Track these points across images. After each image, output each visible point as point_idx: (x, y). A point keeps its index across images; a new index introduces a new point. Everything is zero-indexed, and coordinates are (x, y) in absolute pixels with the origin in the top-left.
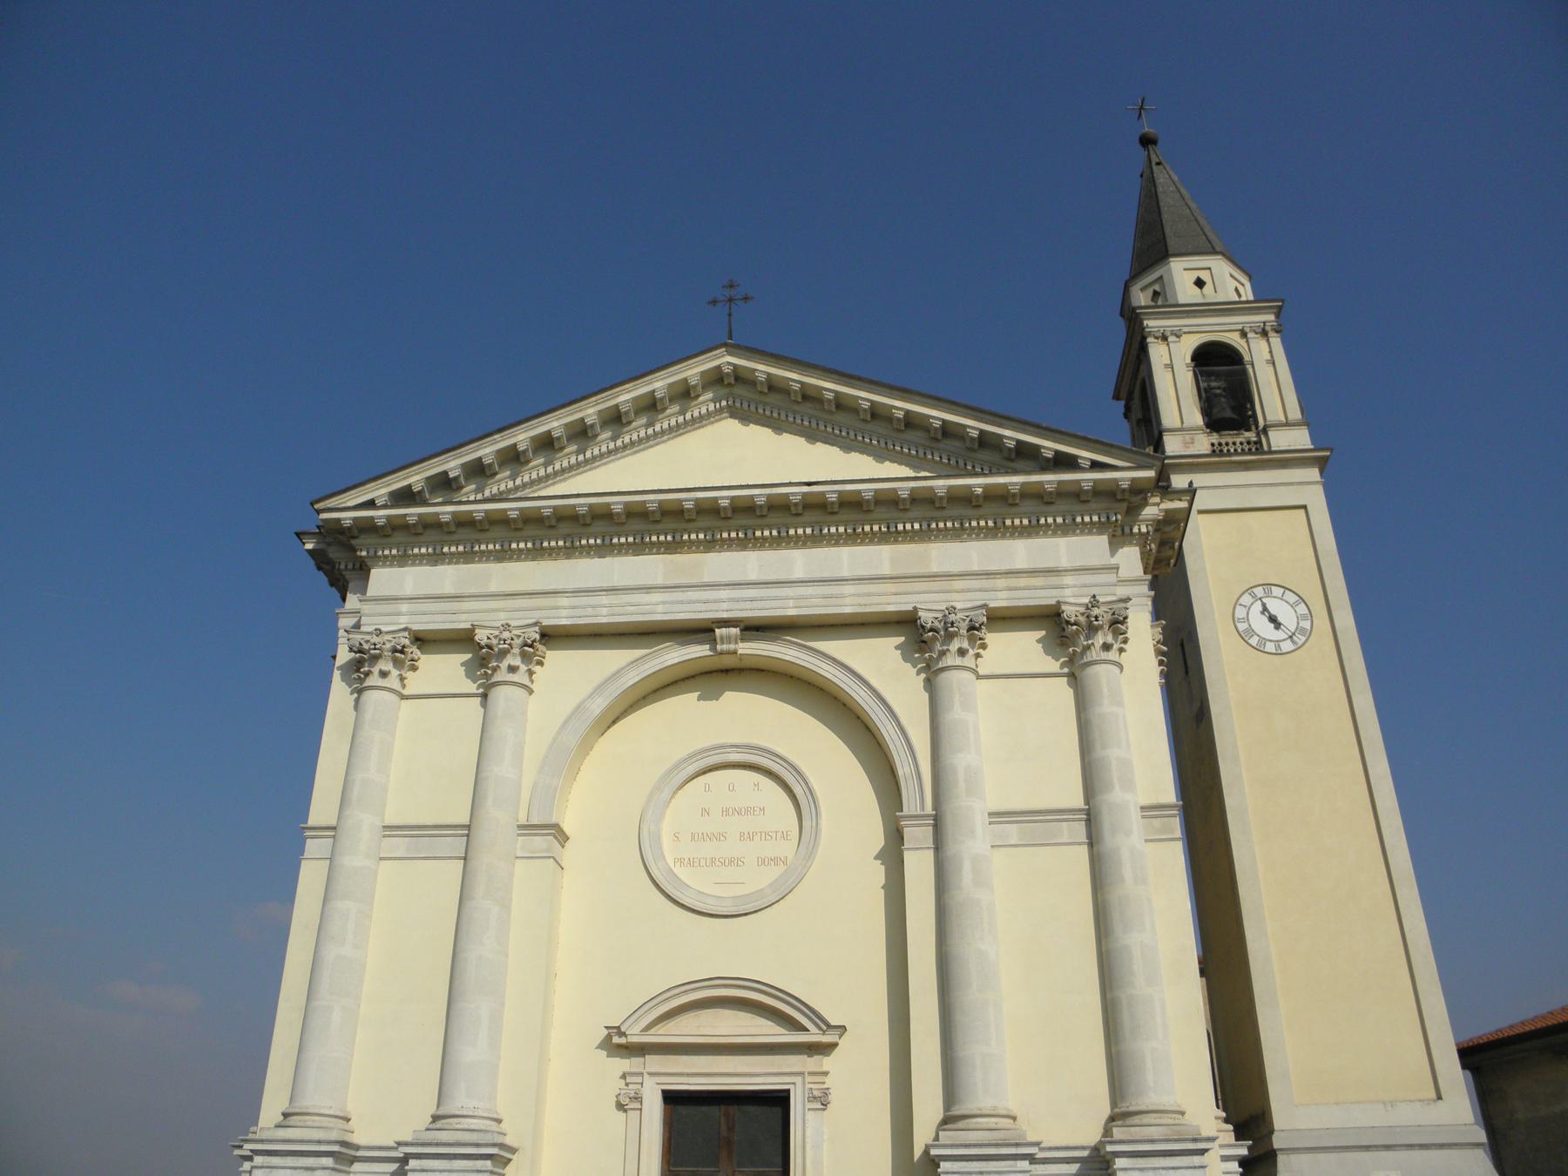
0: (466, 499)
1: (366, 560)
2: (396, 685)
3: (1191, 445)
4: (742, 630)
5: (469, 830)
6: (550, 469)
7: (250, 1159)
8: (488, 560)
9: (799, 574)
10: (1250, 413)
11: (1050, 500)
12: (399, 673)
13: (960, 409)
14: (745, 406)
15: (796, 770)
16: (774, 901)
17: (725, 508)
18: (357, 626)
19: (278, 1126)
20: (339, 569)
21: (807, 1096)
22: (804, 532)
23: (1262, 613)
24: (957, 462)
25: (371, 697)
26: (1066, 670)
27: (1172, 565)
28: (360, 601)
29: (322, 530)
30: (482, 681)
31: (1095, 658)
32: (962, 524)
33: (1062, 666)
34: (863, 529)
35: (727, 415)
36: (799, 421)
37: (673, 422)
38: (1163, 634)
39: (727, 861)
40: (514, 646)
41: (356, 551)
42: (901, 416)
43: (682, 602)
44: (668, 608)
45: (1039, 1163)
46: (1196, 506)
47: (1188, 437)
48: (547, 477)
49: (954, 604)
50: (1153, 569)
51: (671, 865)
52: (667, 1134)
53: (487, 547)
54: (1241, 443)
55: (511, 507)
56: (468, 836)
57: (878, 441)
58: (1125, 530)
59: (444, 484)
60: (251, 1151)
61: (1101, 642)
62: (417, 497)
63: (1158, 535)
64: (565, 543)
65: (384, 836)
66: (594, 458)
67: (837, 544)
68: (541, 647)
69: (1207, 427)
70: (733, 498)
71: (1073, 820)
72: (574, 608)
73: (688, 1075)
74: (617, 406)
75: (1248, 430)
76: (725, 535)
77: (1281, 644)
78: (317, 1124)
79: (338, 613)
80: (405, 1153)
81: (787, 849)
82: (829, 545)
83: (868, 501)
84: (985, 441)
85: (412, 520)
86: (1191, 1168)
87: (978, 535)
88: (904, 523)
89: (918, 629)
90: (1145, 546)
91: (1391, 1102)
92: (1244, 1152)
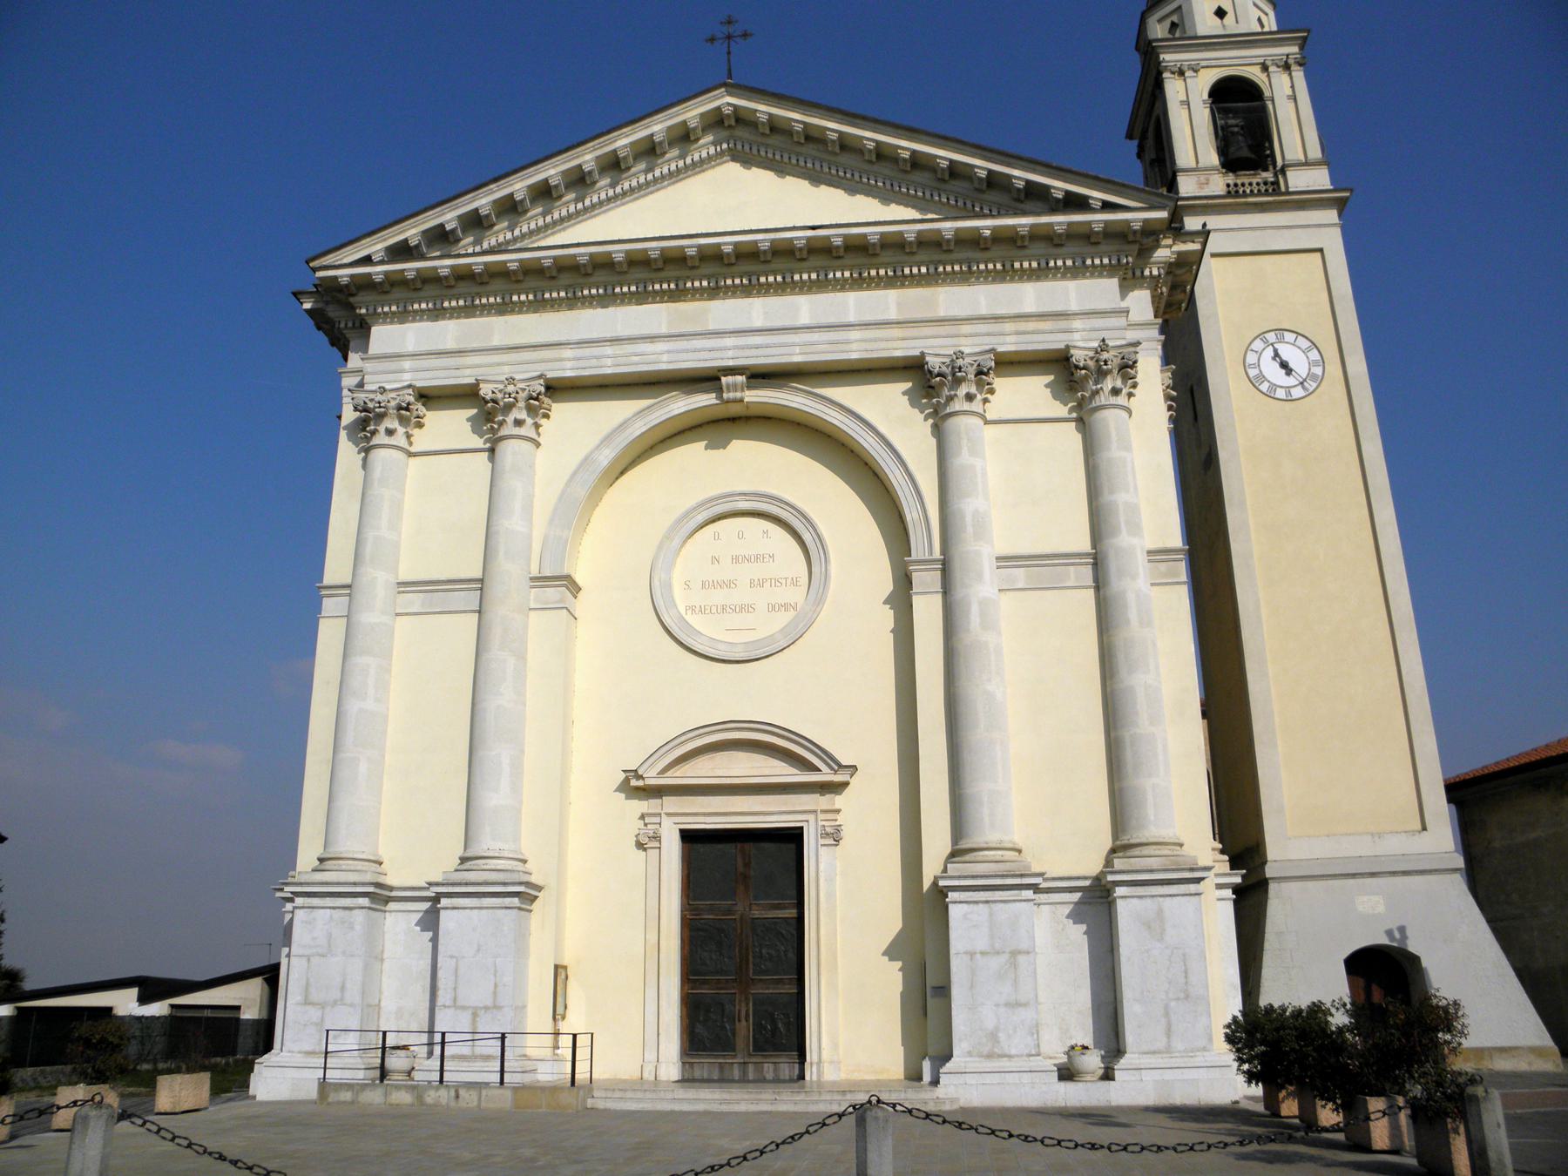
2: (403, 442)
8: (489, 314)
18: (361, 385)
23: (1274, 359)
33: (1070, 411)
35: (729, 158)
43: (687, 351)
47: (1202, 179)
49: (962, 349)
50: (1165, 313)
51: (683, 611)
52: (686, 872)
56: (481, 589)
59: (441, 237)
60: (292, 893)
66: (593, 206)
67: (843, 289)
72: (579, 359)
73: (704, 814)
75: (1266, 170)
81: (797, 595)
82: (834, 290)
84: (994, 182)
85: (410, 275)
88: (911, 267)
90: (1156, 290)
92: (1238, 880)
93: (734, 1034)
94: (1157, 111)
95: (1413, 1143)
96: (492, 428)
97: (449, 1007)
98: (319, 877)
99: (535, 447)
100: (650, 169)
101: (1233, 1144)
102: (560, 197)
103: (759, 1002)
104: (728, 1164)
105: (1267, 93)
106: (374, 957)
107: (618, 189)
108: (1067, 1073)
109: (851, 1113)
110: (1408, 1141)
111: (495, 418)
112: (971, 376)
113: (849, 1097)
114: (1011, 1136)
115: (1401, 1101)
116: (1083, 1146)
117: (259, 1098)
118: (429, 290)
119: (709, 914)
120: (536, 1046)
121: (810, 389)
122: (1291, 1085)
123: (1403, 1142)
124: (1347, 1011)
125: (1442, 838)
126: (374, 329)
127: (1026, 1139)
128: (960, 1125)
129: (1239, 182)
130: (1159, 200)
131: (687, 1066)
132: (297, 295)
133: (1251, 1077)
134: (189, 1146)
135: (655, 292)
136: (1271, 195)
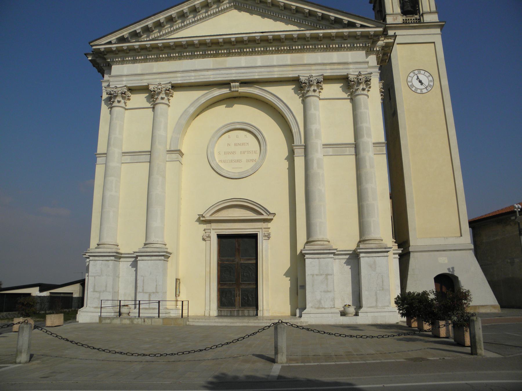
0: (143, 40)
1: (110, 63)
2: (123, 105)
3: (396, 20)
4: (240, 84)
5: (151, 153)
6: (172, 29)
7: (88, 258)
8: (152, 62)
9: (259, 64)
10: (417, 8)
11: (346, 38)
12: (124, 101)
13: (315, 6)
14: (240, 5)
15: (259, 131)
16: (252, 173)
17: (233, 41)
18: (109, 86)
19: (96, 248)
20: (101, 66)
21: (263, 235)
22: (261, 49)
23: (417, 79)
24: (314, 25)
25: (115, 109)
26: (349, 97)
27: (387, 62)
28: (109, 77)
29: (94, 53)
30: (152, 103)
31: (359, 93)
32: (315, 47)
33: (348, 96)
34: (281, 48)
35: (233, 8)
36: (259, 10)
37: (215, 11)
38: (383, 85)
39: (236, 160)
40: (163, 90)
41: (106, 59)
42: (295, 8)
43: (219, 74)
44: (215, 76)
45: (336, 255)
46: (396, 42)
47: (395, 17)
48: (171, 31)
49: (312, 74)
50: (381, 63)
51: (218, 162)
53: (152, 57)
54: (414, 19)
55: (159, 42)
56: (150, 154)
57: (286, 17)
58: (371, 50)
59: (135, 35)
60: (89, 255)
61: (362, 88)
62: (126, 40)
63: (383, 51)
64: (178, 55)
65: (123, 156)
66: (187, 25)
67: (272, 54)
68: (172, 91)
69: (402, 13)
70: (236, 38)
71: (351, 147)
72: (183, 77)
73: (225, 229)
74: (195, 5)
75: (416, 15)
76: (234, 51)
77: (423, 90)
78: (109, 247)
79: (102, 82)
80: (137, 255)
81: (256, 156)
82: (269, 54)
83: (283, 38)
84: (324, 17)
85: (125, 48)
86: (383, 256)
88: (295, 46)
89: (300, 83)
90: (378, 55)
91: (447, 237)
92: (400, 252)
93: (235, 301)
96: (153, 100)
97: (141, 292)
106: (116, 276)
108: (343, 314)
110: (451, 334)
111: (154, 97)
112: (315, 84)
114: (325, 333)
115: (450, 322)
116: (348, 336)
119: (226, 262)
120: (170, 305)
122: (415, 317)
124: (434, 294)
125: (467, 239)
128: (308, 329)
133: (403, 315)
134: (57, 336)
135: (208, 54)
136: (417, 23)
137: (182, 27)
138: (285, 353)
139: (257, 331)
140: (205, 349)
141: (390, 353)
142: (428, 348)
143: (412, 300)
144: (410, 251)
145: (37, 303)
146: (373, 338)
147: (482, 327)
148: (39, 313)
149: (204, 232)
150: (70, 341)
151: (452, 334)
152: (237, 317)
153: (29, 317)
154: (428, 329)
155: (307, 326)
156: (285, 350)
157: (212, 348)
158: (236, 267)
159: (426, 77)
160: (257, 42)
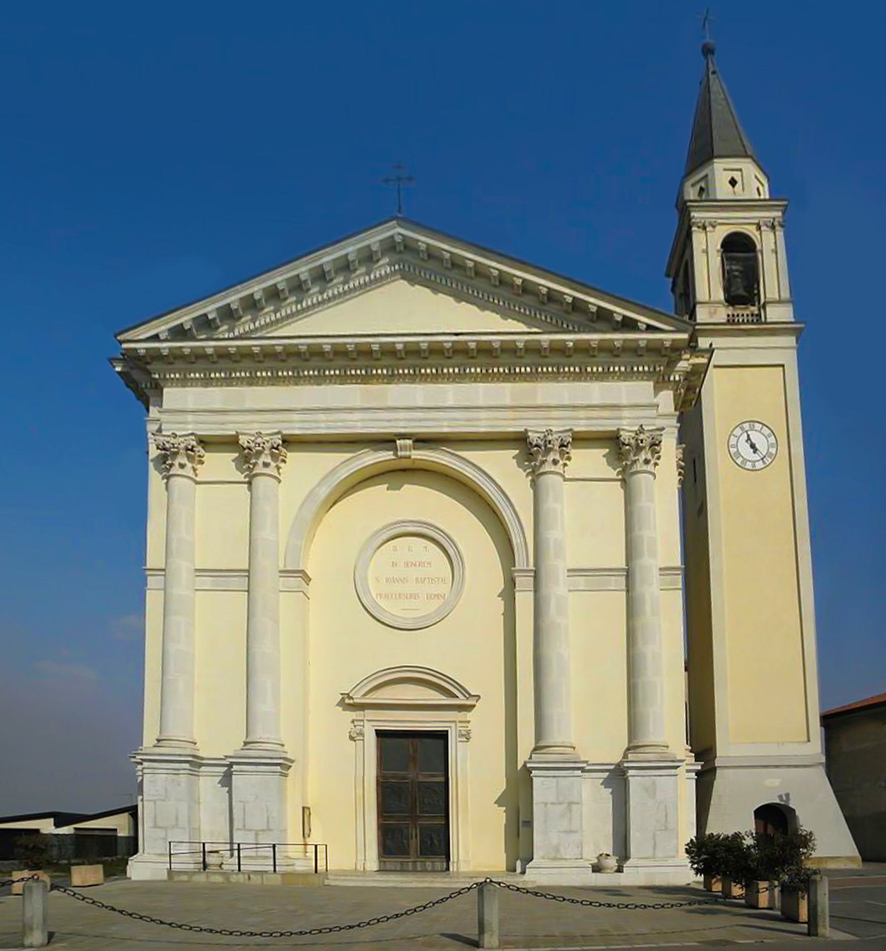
2: (191, 474)
8: (242, 385)
18: (160, 430)
19: (155, 746)
23: (747, 441)
25: (173, 480)
26: (620, 477)
28: (159, 412)
33: (618, 474)
34: (493, 370)
38: (684, 454)
47: (712, 309)
48: (277, 321)
49: (551, 428)
50: (681, 407)
51: (374, 597)
56: (248, 576)
59: (205, 324)
60: (141, 759)
65: (280, 576)
66: (308, 308)
67: (475, 381)
75: (753, 305)
81: (445, 589)
84: (577, 306)
85: (187, 351)
87: (568, 378)
90: (677, 391)
92: (699, 768)
93: (409, 846)
94: (687, 256)
95: (780, 904)
96: (249, 467)
98: (157, 750)
99: (277, 483)
100: (346, 282)
101: (685, 905)
102: (286, 299)
103: (423, 829)
104: (406, 913)
105: (759, 247)
106: (194, 801)
107: (325, 296)
108: (597, 869)
109: (475, 887)
110: (778, 903)
111: (250, 460)
112: (557, 448)
113: (474, 879)
114: (564, 900)
115: (776, 883)
116: (604, 905)
117: (133, 878)
118: (201, 364)
120: (295, 852)
121: (452, 451)
122: (719, 875)
123: (774, 904)
124: (753, 837)
125: (815, 748)
126: (165, 390)
127: (573, 901)
128: (536, 894)
129: (736, 314)
130: (682, 324)
131: (382, 863)
132: (112, 360)
133: (698, 871)
134: (94, 902)
136: (755, 324)
137: (298, 312)
138: (497, 932)
139: (448, 896)
140: (359, 925)
141: (673, 932)
142: (737, 925)
143: (715, 847)
144: (716, 765)
145: (52, 846)
146: (646, 909)
147: (830, 891)
148: (57, 863)
149: (352, 724)
150: (119, 911)
151: (778, 903)
152: (414, 873)
153: (39, 869)
154: (738, 894)
155: (534, 888)
156: (495, 926)
157: (371, 923)
158: (410, 789)
159: (763, 437)
160: (446, 354)
